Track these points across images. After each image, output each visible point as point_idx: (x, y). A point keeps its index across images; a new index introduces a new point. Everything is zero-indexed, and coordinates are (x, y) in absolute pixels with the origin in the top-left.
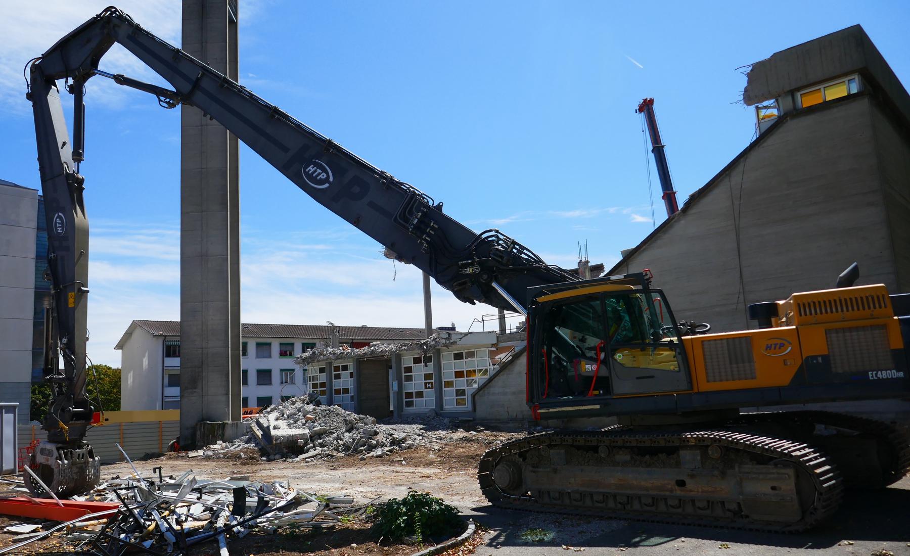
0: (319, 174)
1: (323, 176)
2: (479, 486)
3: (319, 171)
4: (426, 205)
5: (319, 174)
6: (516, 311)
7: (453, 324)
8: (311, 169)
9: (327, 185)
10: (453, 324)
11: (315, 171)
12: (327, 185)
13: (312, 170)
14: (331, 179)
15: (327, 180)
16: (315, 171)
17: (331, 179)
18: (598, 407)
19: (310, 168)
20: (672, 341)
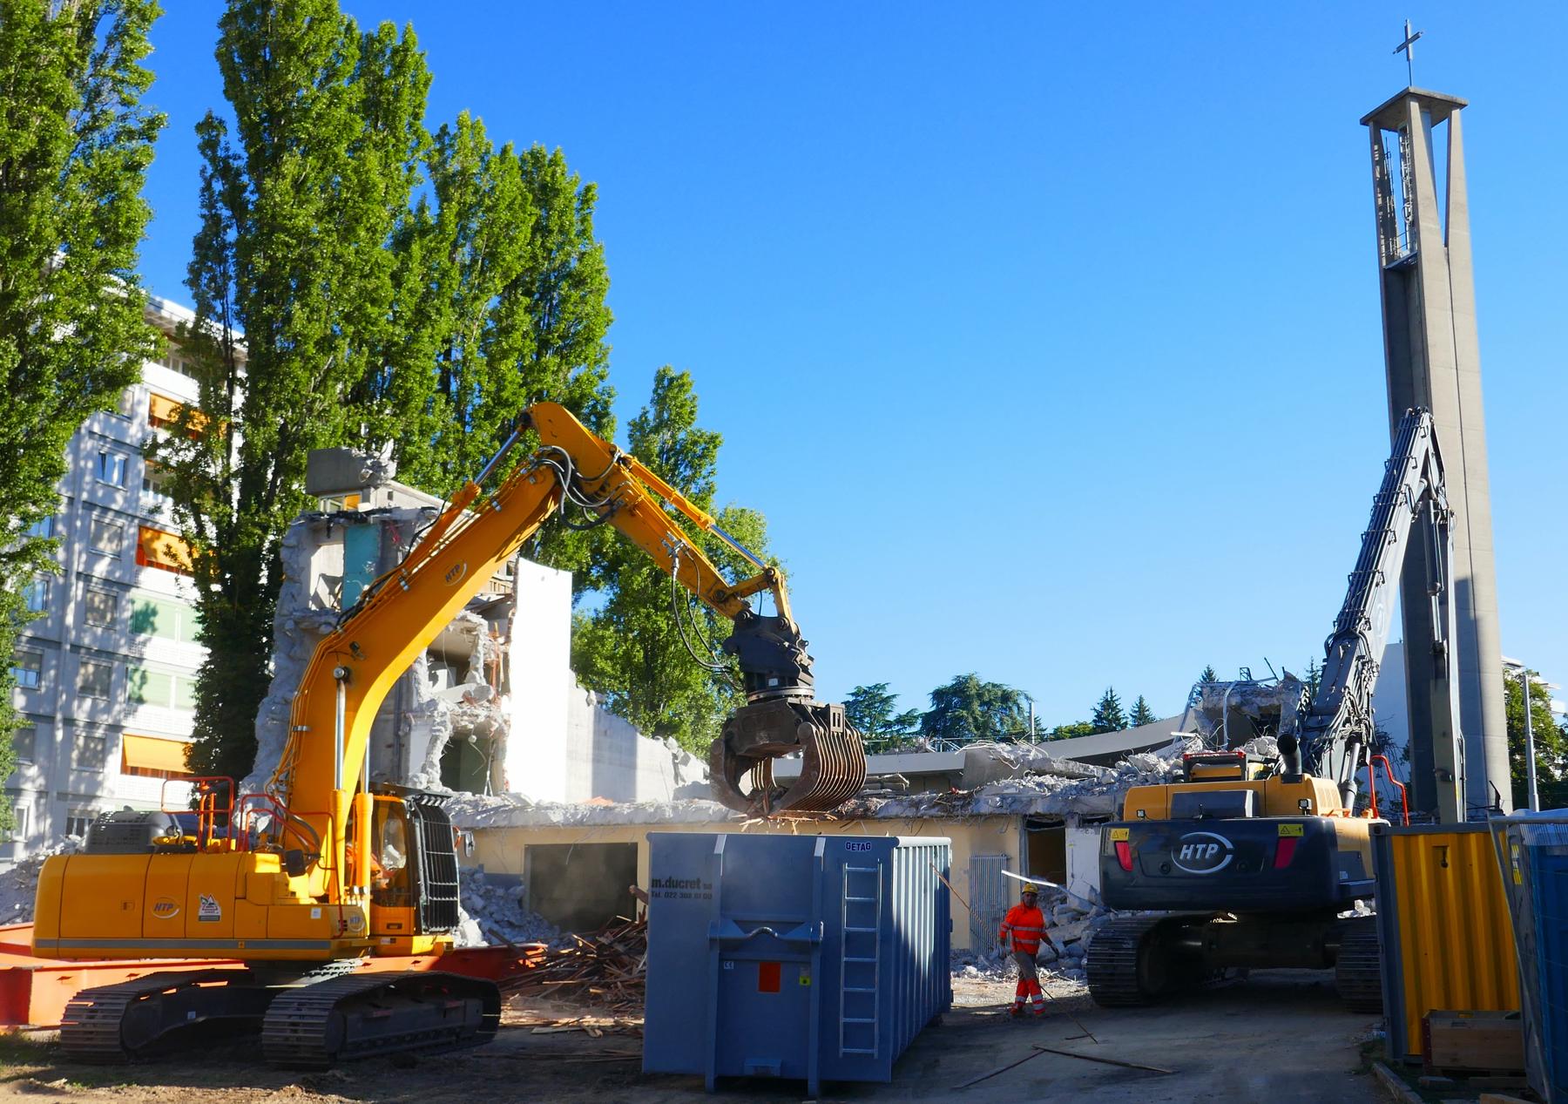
0: (1205, 851)
1: (1213, 849)
2: (194, 713)
3: (1200, 847)
4: (203, 699)
5: (1205, 851)
6: (1522, 694)
7: (1364, 122)
8: (1186, 852)
9: (1228, 858)
10: (1364, 122)
11: (1195, 850)
12: (1228, 858)
13: (1190, 852)
14: (1229, 845)
15: (1223, 851)
16: (1195, 850)
17: (1229, 845)
18: (241, 966)
19: (1184, 851)
20: (450, 957)
